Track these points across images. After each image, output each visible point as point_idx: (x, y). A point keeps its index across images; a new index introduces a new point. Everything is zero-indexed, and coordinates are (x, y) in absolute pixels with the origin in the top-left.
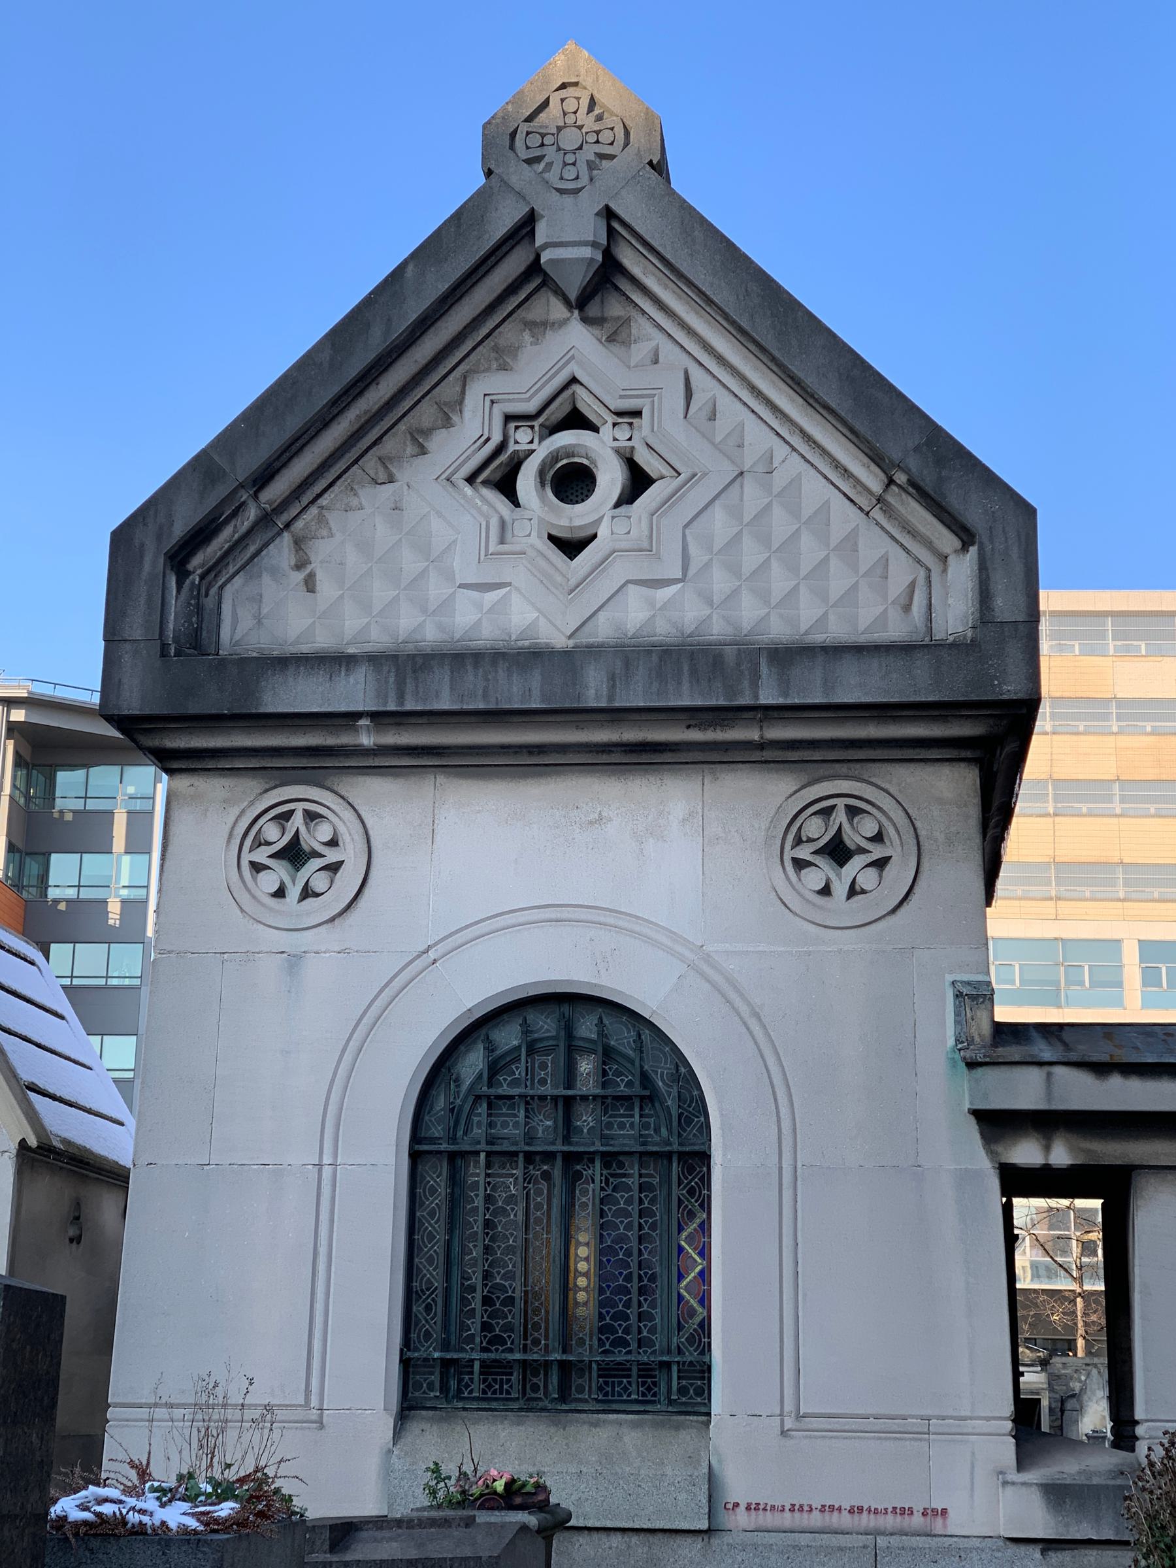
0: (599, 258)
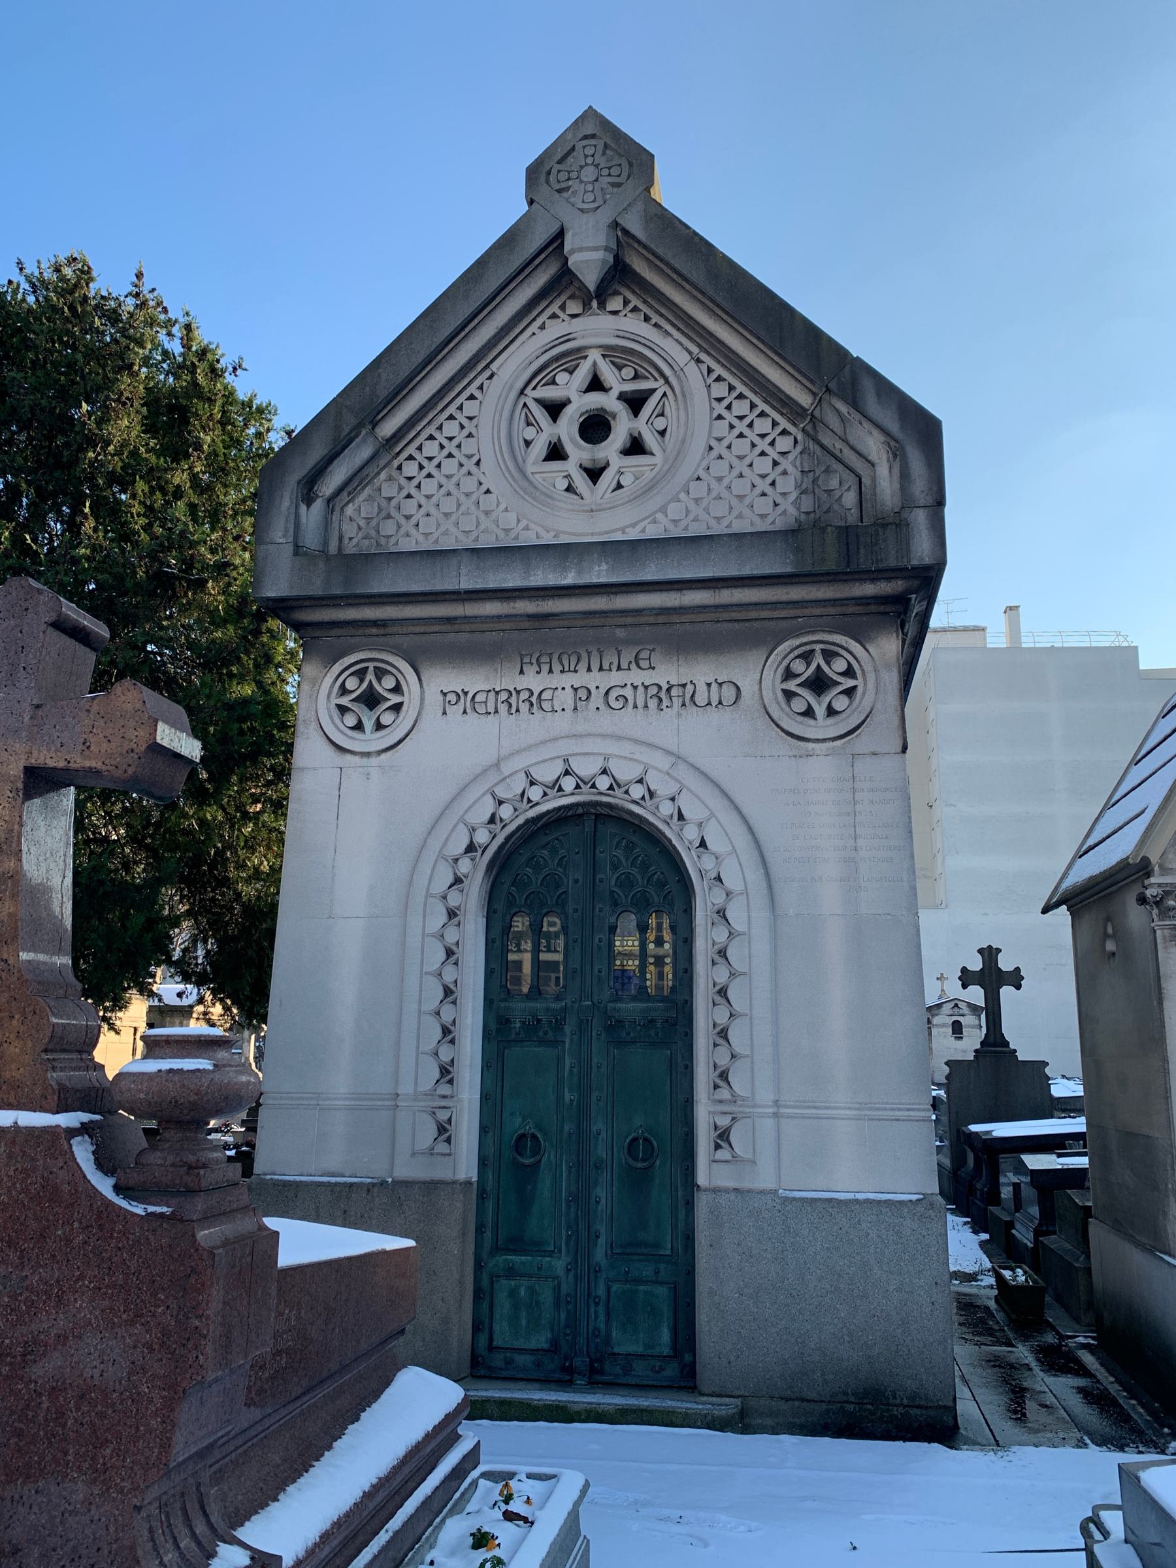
0: (611, 260)
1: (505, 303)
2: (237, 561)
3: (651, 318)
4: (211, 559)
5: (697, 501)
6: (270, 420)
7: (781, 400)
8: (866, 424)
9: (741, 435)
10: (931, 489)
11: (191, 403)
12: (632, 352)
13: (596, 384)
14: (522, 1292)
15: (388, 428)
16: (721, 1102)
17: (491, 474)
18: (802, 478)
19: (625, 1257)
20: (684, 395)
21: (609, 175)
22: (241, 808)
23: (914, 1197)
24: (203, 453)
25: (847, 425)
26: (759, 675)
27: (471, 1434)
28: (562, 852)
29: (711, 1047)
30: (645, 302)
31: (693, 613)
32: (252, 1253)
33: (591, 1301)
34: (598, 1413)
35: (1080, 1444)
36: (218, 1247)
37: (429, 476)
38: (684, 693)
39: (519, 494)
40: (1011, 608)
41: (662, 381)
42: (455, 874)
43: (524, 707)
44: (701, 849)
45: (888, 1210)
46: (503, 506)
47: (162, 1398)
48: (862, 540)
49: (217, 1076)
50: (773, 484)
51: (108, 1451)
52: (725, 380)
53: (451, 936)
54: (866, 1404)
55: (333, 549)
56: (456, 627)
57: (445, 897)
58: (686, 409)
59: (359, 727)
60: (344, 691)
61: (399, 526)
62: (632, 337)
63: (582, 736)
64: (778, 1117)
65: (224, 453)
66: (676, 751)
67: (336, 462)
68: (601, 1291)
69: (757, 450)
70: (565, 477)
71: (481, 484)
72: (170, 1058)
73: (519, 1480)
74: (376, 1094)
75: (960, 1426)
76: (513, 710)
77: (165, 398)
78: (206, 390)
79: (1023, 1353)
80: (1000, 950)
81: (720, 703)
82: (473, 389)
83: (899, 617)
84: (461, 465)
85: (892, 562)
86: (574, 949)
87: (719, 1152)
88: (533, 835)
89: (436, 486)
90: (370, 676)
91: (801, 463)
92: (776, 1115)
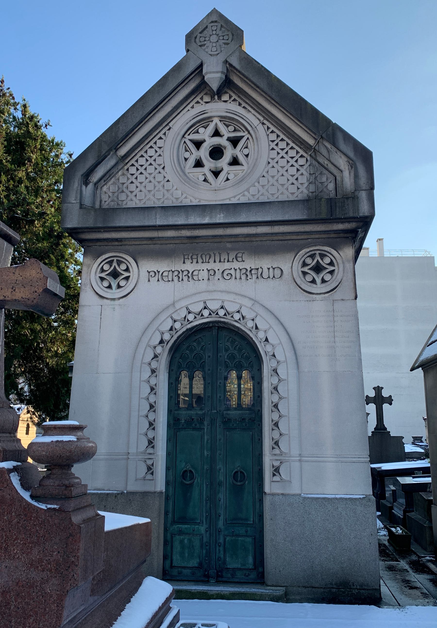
0: (224, 77)
1: (176, 96)
2: (48, 212)
3: (242, 104)
4: (37, 211)
5: (263, 186)
6: (62, 149)
7: (301, 142)
8: (339, 153)
9: (282, 157)
10: (368, 182)
11: (26, 140)
12: (233, 119)
13: (217, 133)
14: (186, 541)
15: (123, 151)
16: (275, 455)
17: (169, 173)
18: (310, 177)
19: (232, 525)
20: (257, 139)
21: (223, 39)
22: (49, 324)
23: (362, 497)
24: (32, 163)
25: (330, 153)
26: (291, 265)
27: (176, 606)
28: (203, 344)
29: (271, 431)
30: (239, 97)
31: (261, 237)
32: (95, 526)
33: (217, 545)
34: (221, 595)
35: (435, 604)
36: (82, 524)
37: (141, 173)
38: (257, 272)
39: (182, 182)
40: (380, 240)
41: (246, 133)
42: (155, 353)
43: (185, 278)
44: (266, 342)
45: (350, 502)
46: (175, 188)
47: (57, 595)
48: (337, 204)
49: (79, 443)
50: (297, 179)
51: (31, 621)
52: (275, 132)
53: (153, 381)
54: (341, 588)
55: (97, 206)
56: (154, 242)
57: (150, 364)
58: (258, 145)
59: (110, 287)
60: (103, 270)
61: (127, 196)
62: (233, 112)
63: (212, 291)
64: (301, 462)
65: (41, 164)
66: (254, 299)
67: (99, 166)
68: (221, 541)
69: (290, 164)
70: (203, 175)
71: (165, 177)
72: (56, 435)
73: (199, 627)
74: (118, 453)
75: (382, 597)
76: (180, 280)
77: (14, 138)
78: (34, 134)
79: (403, 564)
80: (383, 388)
81: (274, 277)
82: (161, 135)
83: (353, 239)
84: (156, 169)
85: (351, 215)
86: (208, 387)
87: (275, 477)
88: (190, 335)
89: (144, 178)
90: (115, 264)
91: (310, 170)
92: (300, 461)
